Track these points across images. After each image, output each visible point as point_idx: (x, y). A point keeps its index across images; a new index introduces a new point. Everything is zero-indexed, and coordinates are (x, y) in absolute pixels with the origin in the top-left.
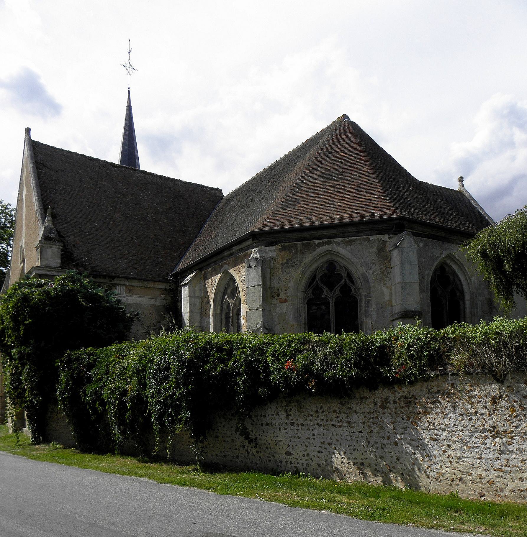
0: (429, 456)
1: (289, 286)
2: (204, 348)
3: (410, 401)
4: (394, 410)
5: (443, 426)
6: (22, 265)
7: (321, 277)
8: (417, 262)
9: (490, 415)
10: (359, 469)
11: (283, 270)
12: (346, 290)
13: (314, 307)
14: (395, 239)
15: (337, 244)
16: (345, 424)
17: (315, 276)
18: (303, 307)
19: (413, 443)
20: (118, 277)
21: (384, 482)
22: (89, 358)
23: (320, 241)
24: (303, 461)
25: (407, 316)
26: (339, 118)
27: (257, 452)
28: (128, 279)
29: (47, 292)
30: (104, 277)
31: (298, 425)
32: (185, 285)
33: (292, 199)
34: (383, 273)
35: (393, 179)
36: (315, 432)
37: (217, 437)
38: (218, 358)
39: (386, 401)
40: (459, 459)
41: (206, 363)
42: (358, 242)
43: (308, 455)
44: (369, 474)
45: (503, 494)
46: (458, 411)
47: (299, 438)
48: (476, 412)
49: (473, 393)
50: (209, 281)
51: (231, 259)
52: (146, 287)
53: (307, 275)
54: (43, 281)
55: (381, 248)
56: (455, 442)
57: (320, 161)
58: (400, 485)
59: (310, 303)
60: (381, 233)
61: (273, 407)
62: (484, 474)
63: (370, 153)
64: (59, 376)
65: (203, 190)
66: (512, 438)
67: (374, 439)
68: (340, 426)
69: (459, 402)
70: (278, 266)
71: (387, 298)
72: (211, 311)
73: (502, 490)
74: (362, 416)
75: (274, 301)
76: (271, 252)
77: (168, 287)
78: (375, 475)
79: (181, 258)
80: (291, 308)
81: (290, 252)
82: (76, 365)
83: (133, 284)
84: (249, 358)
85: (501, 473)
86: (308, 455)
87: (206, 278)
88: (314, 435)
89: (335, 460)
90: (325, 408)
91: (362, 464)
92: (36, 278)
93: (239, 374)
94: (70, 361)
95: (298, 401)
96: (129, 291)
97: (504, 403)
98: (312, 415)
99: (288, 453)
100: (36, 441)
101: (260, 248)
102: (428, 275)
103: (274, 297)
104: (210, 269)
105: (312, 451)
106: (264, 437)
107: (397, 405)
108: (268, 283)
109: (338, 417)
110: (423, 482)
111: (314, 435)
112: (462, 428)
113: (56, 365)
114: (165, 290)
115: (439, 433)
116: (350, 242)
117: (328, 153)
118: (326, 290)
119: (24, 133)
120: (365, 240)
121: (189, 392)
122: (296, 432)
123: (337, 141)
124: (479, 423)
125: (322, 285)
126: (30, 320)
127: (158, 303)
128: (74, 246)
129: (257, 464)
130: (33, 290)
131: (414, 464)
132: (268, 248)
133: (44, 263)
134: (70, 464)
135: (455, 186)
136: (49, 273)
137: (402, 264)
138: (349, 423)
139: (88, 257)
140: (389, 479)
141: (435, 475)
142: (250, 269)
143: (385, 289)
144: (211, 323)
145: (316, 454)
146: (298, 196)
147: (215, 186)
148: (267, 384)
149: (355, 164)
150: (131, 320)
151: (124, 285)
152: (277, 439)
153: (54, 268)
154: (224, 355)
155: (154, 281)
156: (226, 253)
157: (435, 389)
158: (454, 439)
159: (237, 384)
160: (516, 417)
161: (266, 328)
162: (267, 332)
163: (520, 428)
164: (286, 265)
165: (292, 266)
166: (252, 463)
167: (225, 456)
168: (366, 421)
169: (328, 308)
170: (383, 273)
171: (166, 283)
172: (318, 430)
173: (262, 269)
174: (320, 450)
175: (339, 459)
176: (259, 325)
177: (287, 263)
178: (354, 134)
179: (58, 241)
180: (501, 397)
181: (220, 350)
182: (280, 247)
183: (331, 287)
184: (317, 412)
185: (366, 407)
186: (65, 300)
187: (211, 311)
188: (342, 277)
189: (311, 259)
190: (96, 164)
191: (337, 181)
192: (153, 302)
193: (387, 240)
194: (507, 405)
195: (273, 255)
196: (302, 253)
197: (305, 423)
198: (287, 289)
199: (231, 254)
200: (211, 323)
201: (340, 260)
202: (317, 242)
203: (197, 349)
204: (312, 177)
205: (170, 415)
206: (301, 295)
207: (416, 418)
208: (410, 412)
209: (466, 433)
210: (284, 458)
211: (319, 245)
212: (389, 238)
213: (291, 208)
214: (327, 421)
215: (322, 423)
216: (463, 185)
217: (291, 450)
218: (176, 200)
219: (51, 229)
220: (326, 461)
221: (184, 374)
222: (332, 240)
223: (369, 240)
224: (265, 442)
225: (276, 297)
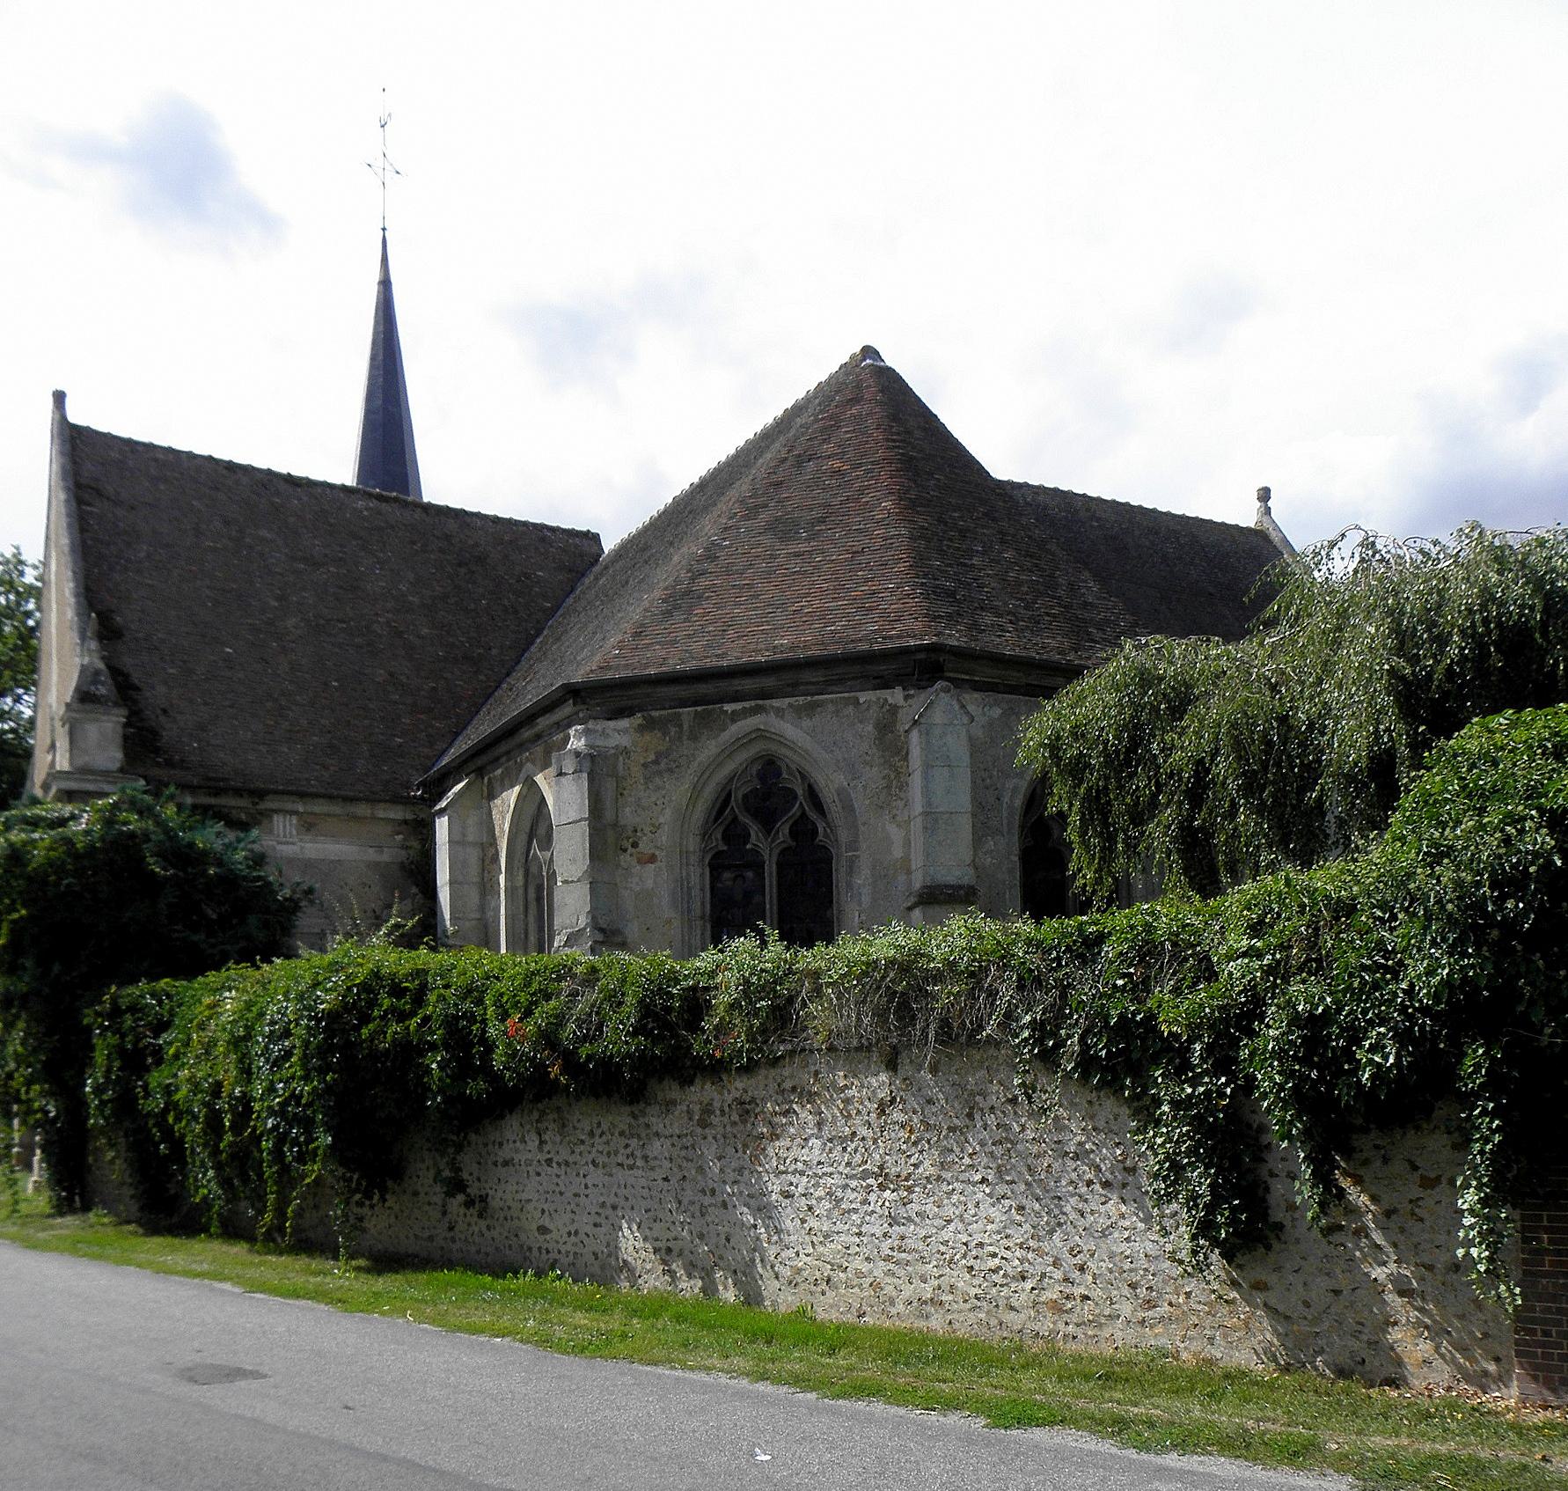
0: (778, 1231)
1: (662, 820)
2: (365, 987)
3: (746, 1109)
4: (720, 1129)
5: (800, 1166)
6: (50, 757)
7: (745, 796)
8: (966, 760)
9: (875, 1141)
10: (664, 1262)
11: (648, 779)
12: (804, 831)
13: (727, 875)
14: (921, 699)
15: (779, 712)
16: (639, 1163)
17: (729, 795)
18: (698, 877)
19: (752, 1202)
20: (276, 792)
21: (703, 1290)
22: (160, 1003)
23: (738, 706)
24: (569, 1247)
25: (938, 898)
26: (853, 357)
27: (488, 1227)
28: (303, 796)
29: (68, 842)
30: (238, 792)
31: (559, 1164)
32: (442, 812)
33: (688, 592)
34: (889, 787)
35: (960, 531)
36: (589, 1181)
37: (416, 1194)
38: (392, 1010)
39: (707, 1110)
40: (826, 1236)
41: (365, 1019)
42: (831, 707)
43: (576, 1233)
44: (681, 1272)
45: (894, 1311)
46: (826, 1133)
47: (561, 1193)
48: (854, 1134)
49: (850, 1093)
50: (498, 801)
51: (539, 750)
52: (355, 818)
53: (710, 792)
54: (68, 810)
55: (886, 725)
56: (820, 1199)
57: (778, 484)
58: (729, 1295)
59: (716, 866)
60: (887, 685)
61: (516, 1124)
62: (865, 1267)
63: (912, 458)
64: (92, 1048)
65: (543, 539)
66: (910, 1190)
67: (688, 1195)
68: (631, 1167)
69: (827, 1114)
70: (636, 770)
71: (898, 853)
72: (502, 879)
73: (892, 1303)
74: (668, 1142)
75: (625, 859)
76: (619, 733)
77: (409, 816)
78: (690, 1276)
79: (457, 734)
80: (665, 879)
81: (664, 734)
82: (128, 1021)
83: (317, 809)
84: (452, 1011)
85: (892, 1266)
86: (576, 1233)
87: (492, 796)
88: (586, 1187)
89: (623, 1245)
90: (605, 1127)
91: (669, 1250)
92: (60, 800)
93: (433, 1047)
94: (116, 1013)
95: (558, 1109)
96: (309, 826)
97: (897, 1116)
98: (583, 1142)
99: (543, 1230)
100: (64, 1207)
101: (591, 725)
102: (1015, 790)
103: (625, 850)
104: (499, 771)
105: (584, 1223)
106: (500, 1193)
107: (725, 1119)
108: (609, 815)
109: (627, 1146)
110: (769, 1287)
111: (586, 1187)
112: (831, 1169)
113: (85, 1021)
114: (405, 822)
115: (795, 1181)
116: (811, 709)
117: (800, 461)
118: (754, 830)
119: (50, 400)
120: (847, 702)
121: (329, 1089)
122: (556, 1180)
123: (830, 426)
124: (858, 1158)
125: (745, 819)
126: (24, 912)
127: (386, 857)
128: (165, 711)
129: (487, 1254)
130: (36, 835)
131: (755, 1250)
132: (611, 724)
133: (80, 762)
134: (100, 1257)
135: (1243, 514)
136: (90, 787)
137: (928, 767)
138: (645, 1158)
139: (199, 741)
140: (713, 1282)
141: (786, 1272)
142: (563, 780)
143: (892, 830)
144: (503, 911)
145: (589, 1229)
146: (703, 582)
147: (581, 527)
148: (486, 1070)
149: (861, 491)
150: (292, 907)
151: (296, 813)
152: (524, 1196)
153: (105, 774)
154: (405, 1004)
155: (372, 800)
156: (527, 733)
157: (788, 1085)
158: (817, 1194)
159: (428, 1071)
160: (915, 1144)
161: (602, 930)
162: (600, 937)
163: (920, 1170)
164: (655, 768)
165: (671, 771)
166: (478, 1252)
167: (431, 1238)
168: (675, 1156)
169: (760, 876)
170: (889, 787)
171: (405, 804)
172: (596, 1176)
173: (591, 780)
174: (598, 1220)
175: (631, 1243)
176: (583, 921)
177: (656, 762)
178: (881, 403)
179: (116, 704)
180: (893, 1101)
181: (397, 991)
182: (640, 721)
183: (768, 821)
184: (592, 1134)
185: (675, 1123)
186: (117, 855)
187: (502, 879)
188: (796, 797)
189: (716, 752)
190: (245, 480)
191: (808, 540)
192: (372, 855)
193: (901, 702)
194: (901, 1117)
195: (625, 741)
196: (694, 738)
197: (571, 1160)
198: (657, 828)
199: (538, 737)
200: (503, 911)
201: (789, 753)
202: (729, 707)
203: (349, 989)
204: (749, 530)
205: (295, 1142)
206: (693, 843)
207: (756, 1145)
208: (748, 1131)
209: (837, 1180)
210: (535, 1240)
211: (735, 717)
212: (906, 698)
213: (678, 616)
214: (609, 1154)
215: (601, 1160)
216: (1268, 511)
217: (546, 1222)
218: (463, 570)
219: (97, 673)
220: (608, 1245)
221: (318, 1047)
222: (767, 702)
223: (856, 702)
224: (501, 1204)
225: (630, 850)
